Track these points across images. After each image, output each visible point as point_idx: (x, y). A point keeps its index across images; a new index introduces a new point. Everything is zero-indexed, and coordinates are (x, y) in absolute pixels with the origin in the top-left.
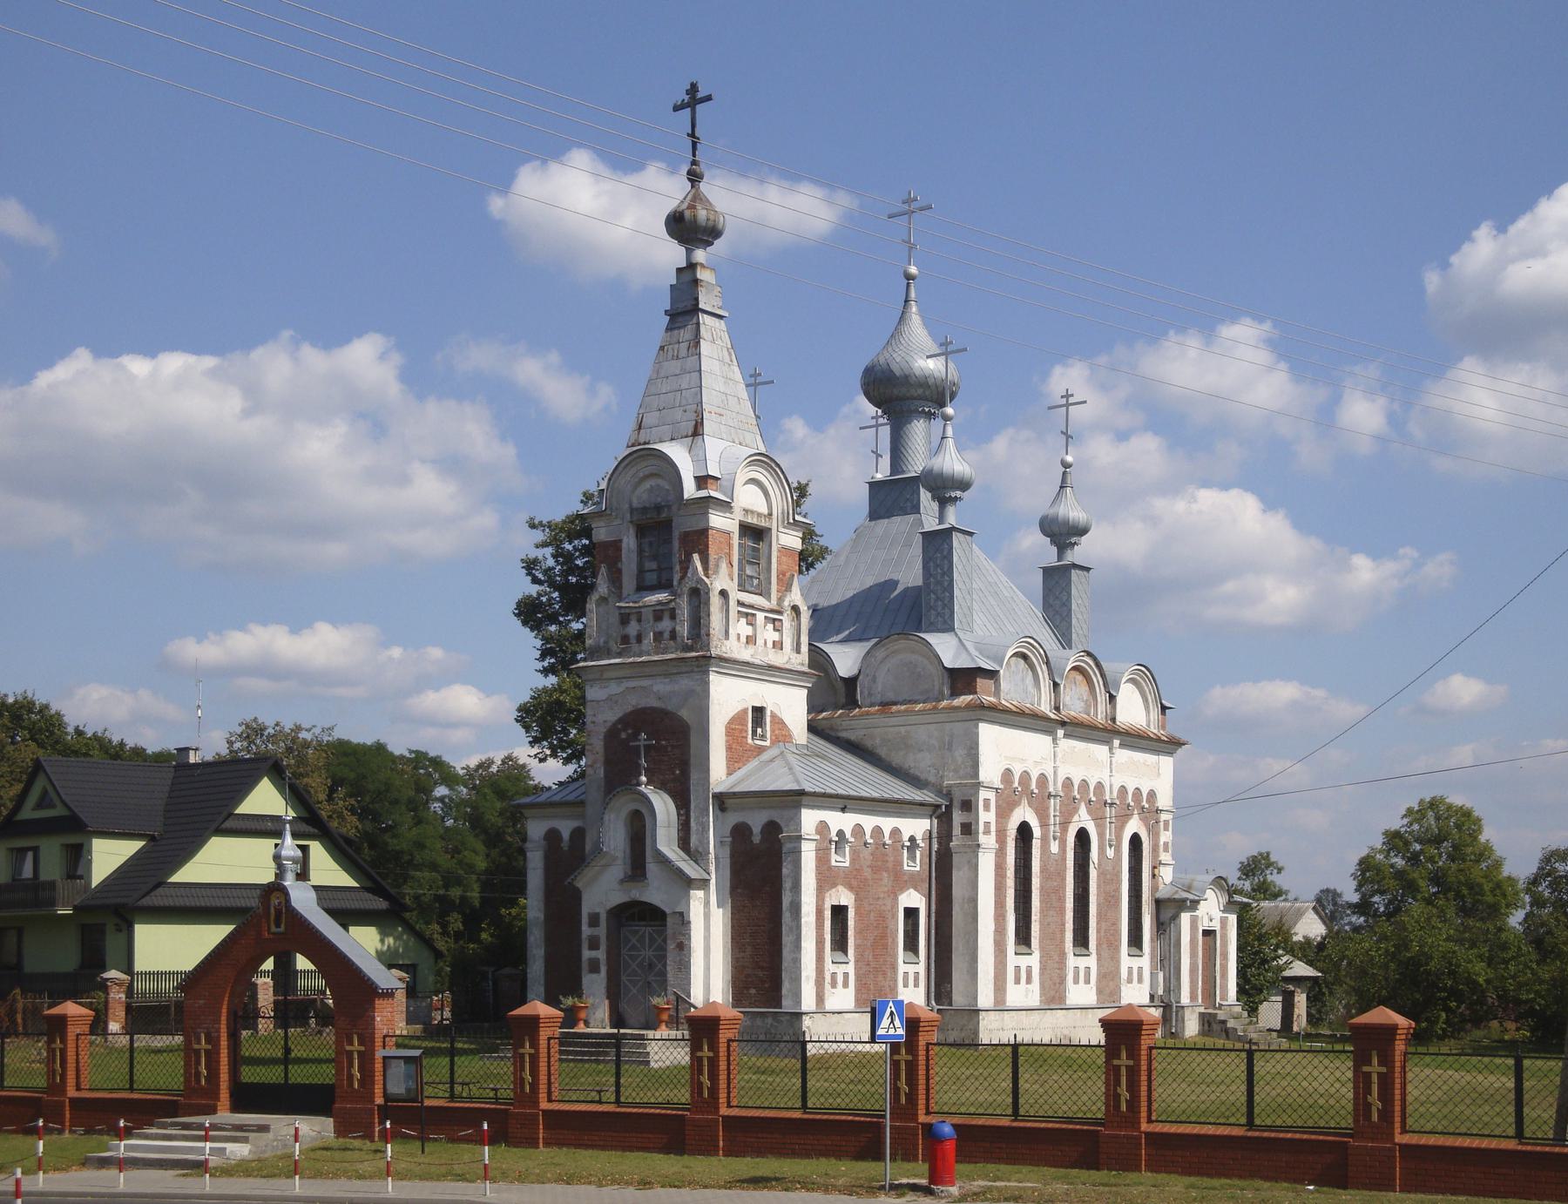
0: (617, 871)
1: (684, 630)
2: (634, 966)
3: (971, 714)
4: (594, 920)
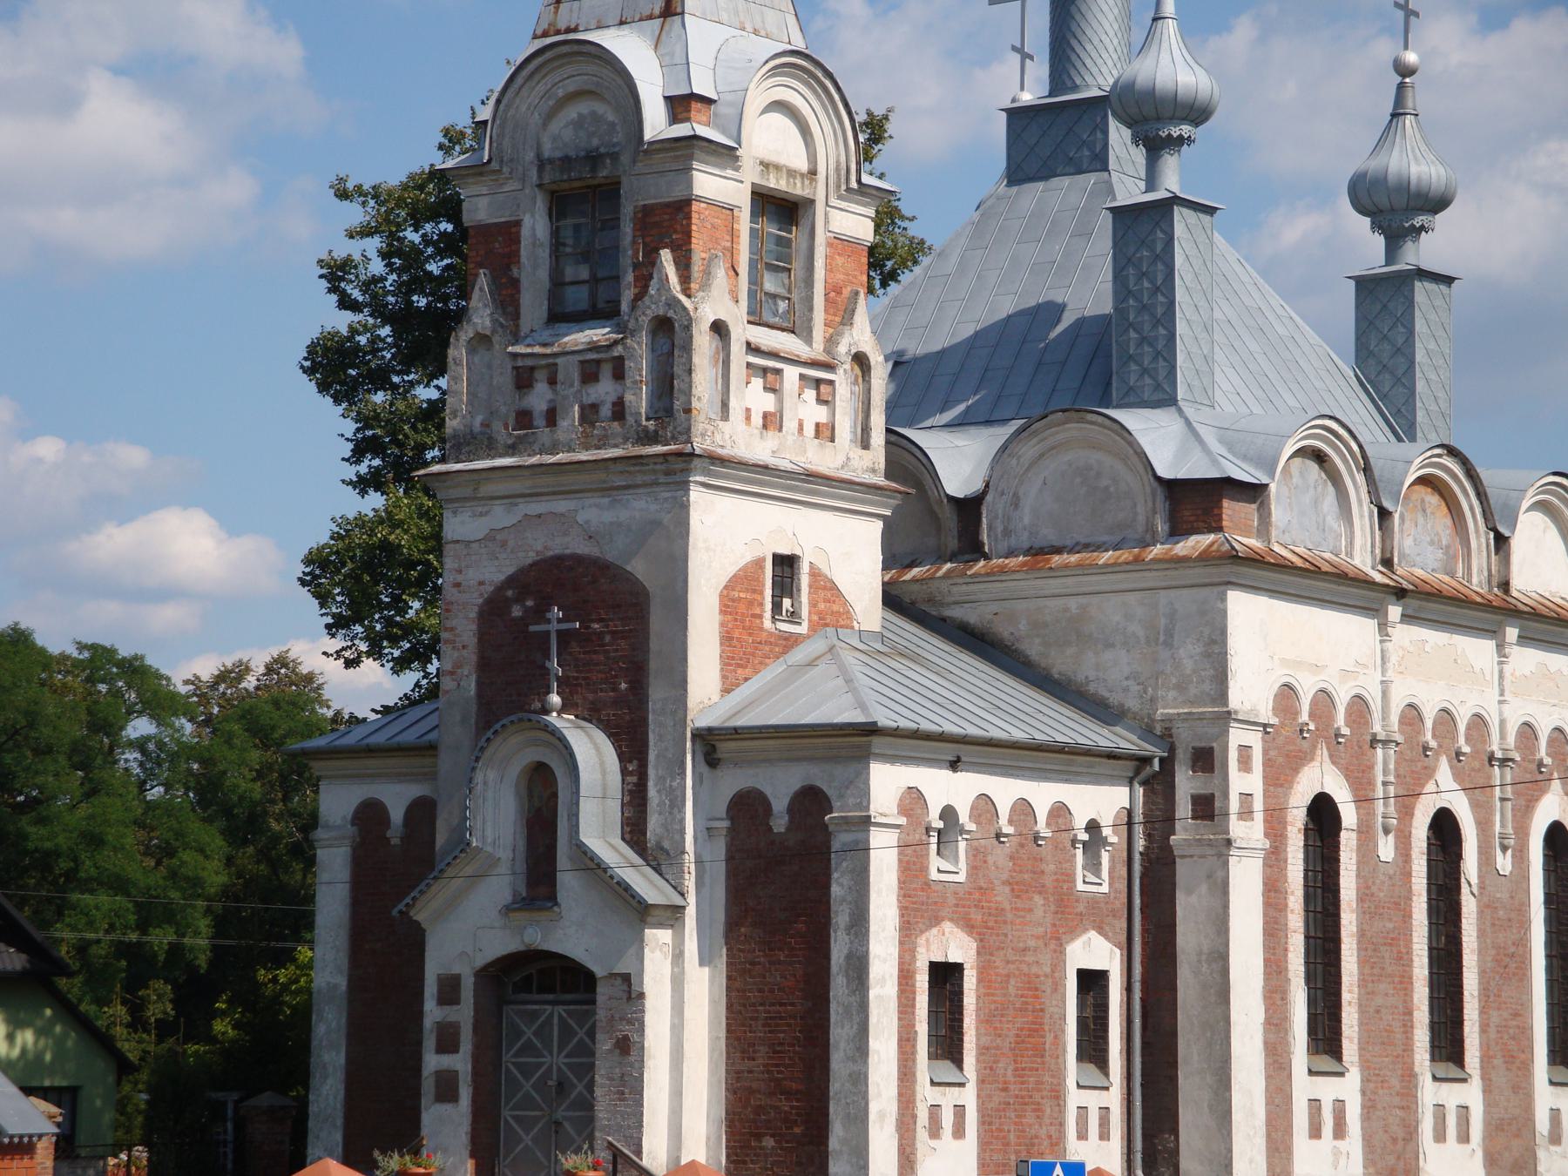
0: (500, 887)
1: (640, 400)
2: (527, 1086)
3: (1214, 573)
4: (449, 990)
